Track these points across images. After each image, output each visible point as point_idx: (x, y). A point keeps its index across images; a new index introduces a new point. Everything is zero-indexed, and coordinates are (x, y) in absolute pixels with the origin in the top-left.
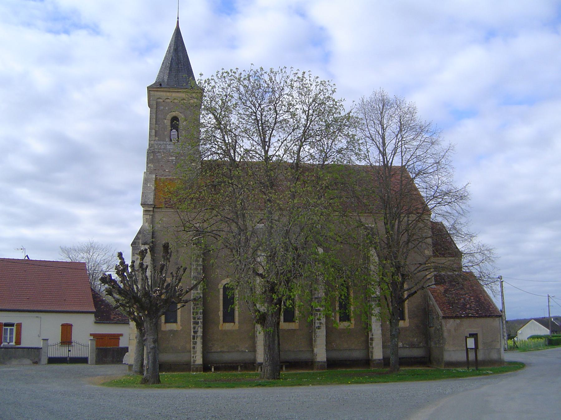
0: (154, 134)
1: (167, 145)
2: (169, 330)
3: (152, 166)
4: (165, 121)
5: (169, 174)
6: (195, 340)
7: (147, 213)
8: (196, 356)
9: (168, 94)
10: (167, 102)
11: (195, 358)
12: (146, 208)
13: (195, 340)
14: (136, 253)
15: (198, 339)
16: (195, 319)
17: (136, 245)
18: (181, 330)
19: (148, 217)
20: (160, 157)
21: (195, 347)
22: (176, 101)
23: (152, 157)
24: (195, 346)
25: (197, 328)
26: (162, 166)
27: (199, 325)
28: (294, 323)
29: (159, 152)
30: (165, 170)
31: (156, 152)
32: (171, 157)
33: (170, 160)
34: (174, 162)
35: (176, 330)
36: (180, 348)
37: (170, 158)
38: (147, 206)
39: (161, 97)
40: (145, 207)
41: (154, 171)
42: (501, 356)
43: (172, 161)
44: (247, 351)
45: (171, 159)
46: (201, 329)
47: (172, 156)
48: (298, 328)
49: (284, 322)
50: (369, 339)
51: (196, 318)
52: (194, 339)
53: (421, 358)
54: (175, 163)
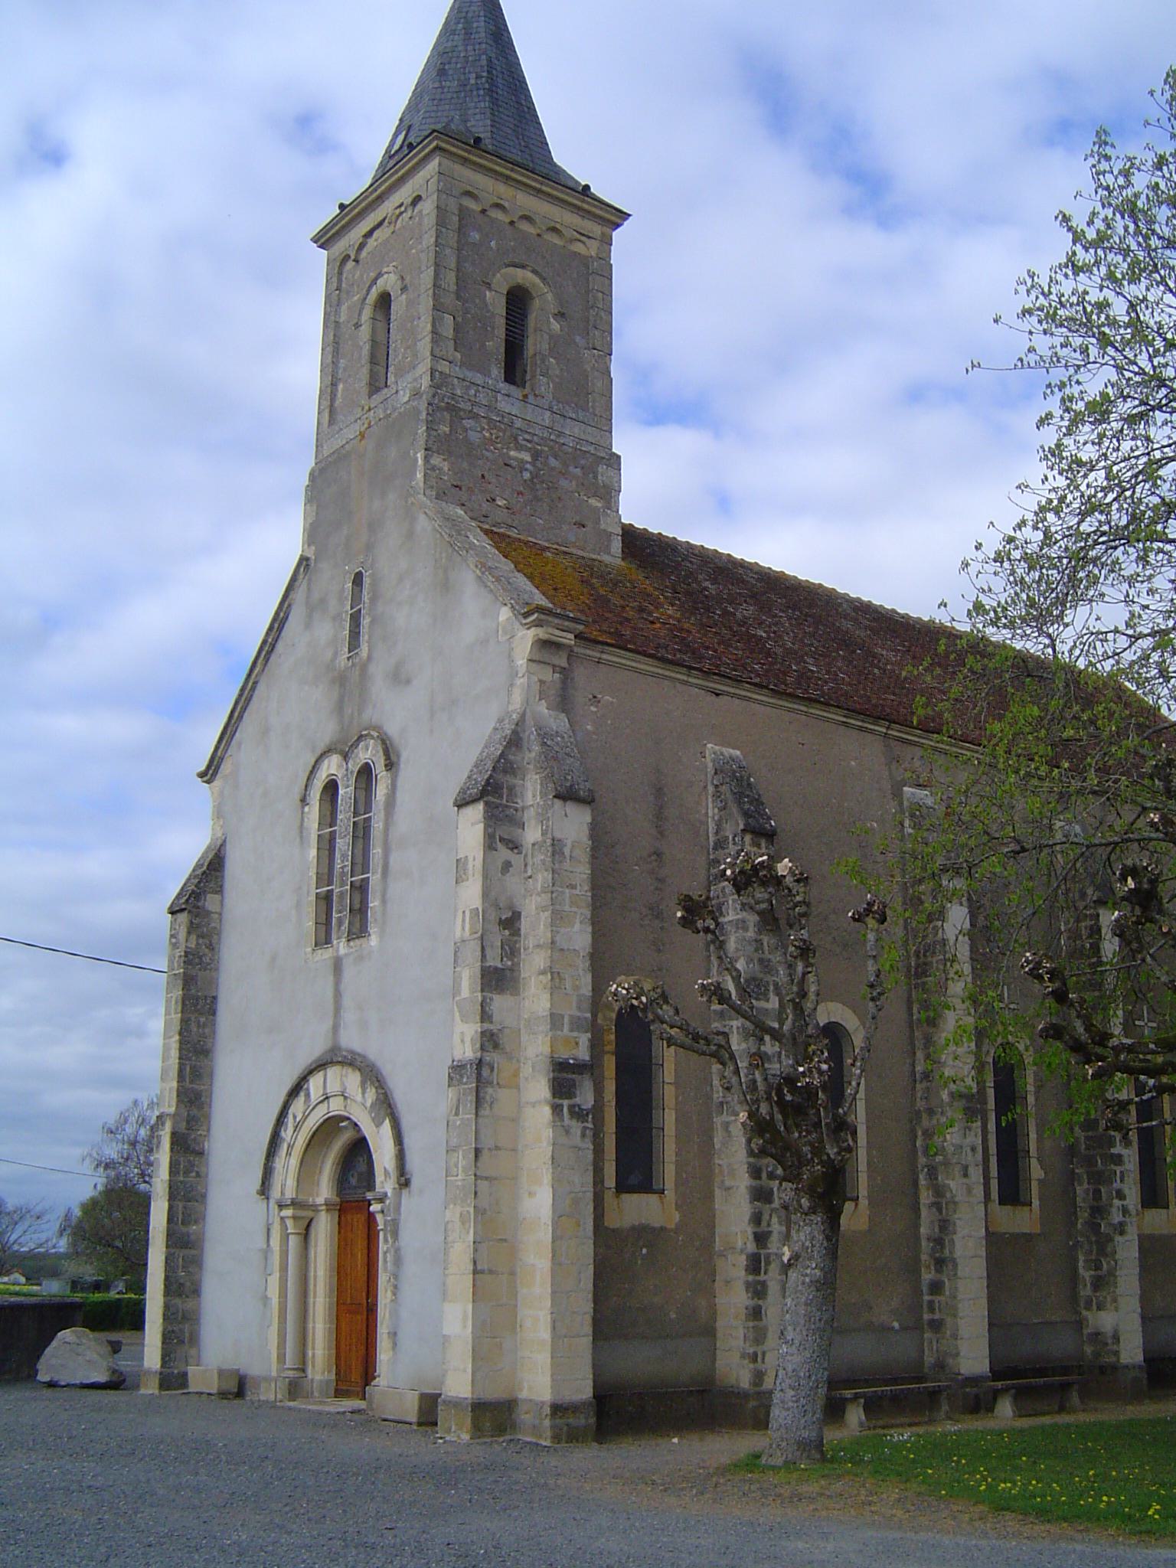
0: (450, 333)
1: (500, 397)
2: (633, 1228)
3: (445, 466)
4: (488, 293)
5: (509, 522)
6: (762, 1277)
7: (546, 657)
8: (764, 1354)
9: (502, 189)
10: (493, 221)
11: (763, 1362)
12: (550, 630)
13: (762, 1277)
14: (501, 839)
15: (770, 1274)
16: (760, 1178)
17: (501, 797)
18: (677, 1230)
19: (548, 675)
20: (474, 436)
21: (760, 1307)
22: (524, 226)
23: (447, 430)
24: (760, 1302)
25: (765, 1217)
26: (483, 476)
27: (773, 1206)
28: (1027, 1209)
29: (475, 417)
30: (494, 500)
31: (460, 409)
32: (517, 449)
33: (514, 463)
34: (527, 475)
35: (657, 1225)
36: (673, 1316)
37: (512, 453)
38: (556, 621)
39: (476, 192)
40: (548, 624)
41: (454, 490)
42: (714, 1360)
43: (522, 466)
44: (896, 1325)
45: (516, 459)
46: (780, 1223)
47: (519, 448)
48: (1039, 1231)
49: (1000, 1204)
50: (925, 1289)
51: (764, 1175)
52: (759, 1273)
53: (107, 1382)
54: (531, 480)
